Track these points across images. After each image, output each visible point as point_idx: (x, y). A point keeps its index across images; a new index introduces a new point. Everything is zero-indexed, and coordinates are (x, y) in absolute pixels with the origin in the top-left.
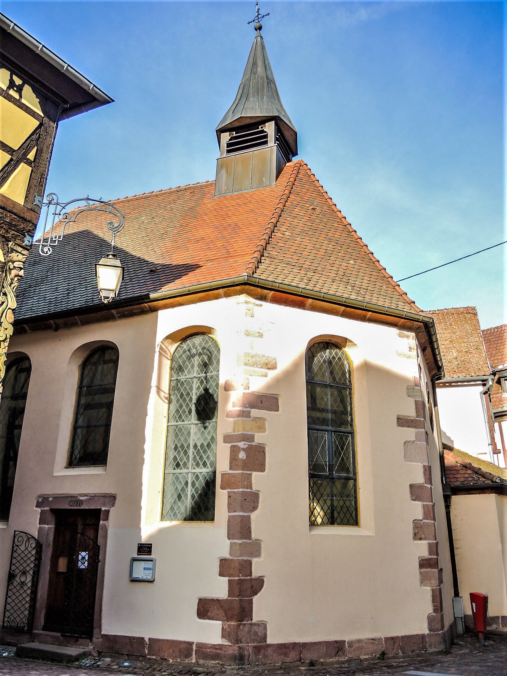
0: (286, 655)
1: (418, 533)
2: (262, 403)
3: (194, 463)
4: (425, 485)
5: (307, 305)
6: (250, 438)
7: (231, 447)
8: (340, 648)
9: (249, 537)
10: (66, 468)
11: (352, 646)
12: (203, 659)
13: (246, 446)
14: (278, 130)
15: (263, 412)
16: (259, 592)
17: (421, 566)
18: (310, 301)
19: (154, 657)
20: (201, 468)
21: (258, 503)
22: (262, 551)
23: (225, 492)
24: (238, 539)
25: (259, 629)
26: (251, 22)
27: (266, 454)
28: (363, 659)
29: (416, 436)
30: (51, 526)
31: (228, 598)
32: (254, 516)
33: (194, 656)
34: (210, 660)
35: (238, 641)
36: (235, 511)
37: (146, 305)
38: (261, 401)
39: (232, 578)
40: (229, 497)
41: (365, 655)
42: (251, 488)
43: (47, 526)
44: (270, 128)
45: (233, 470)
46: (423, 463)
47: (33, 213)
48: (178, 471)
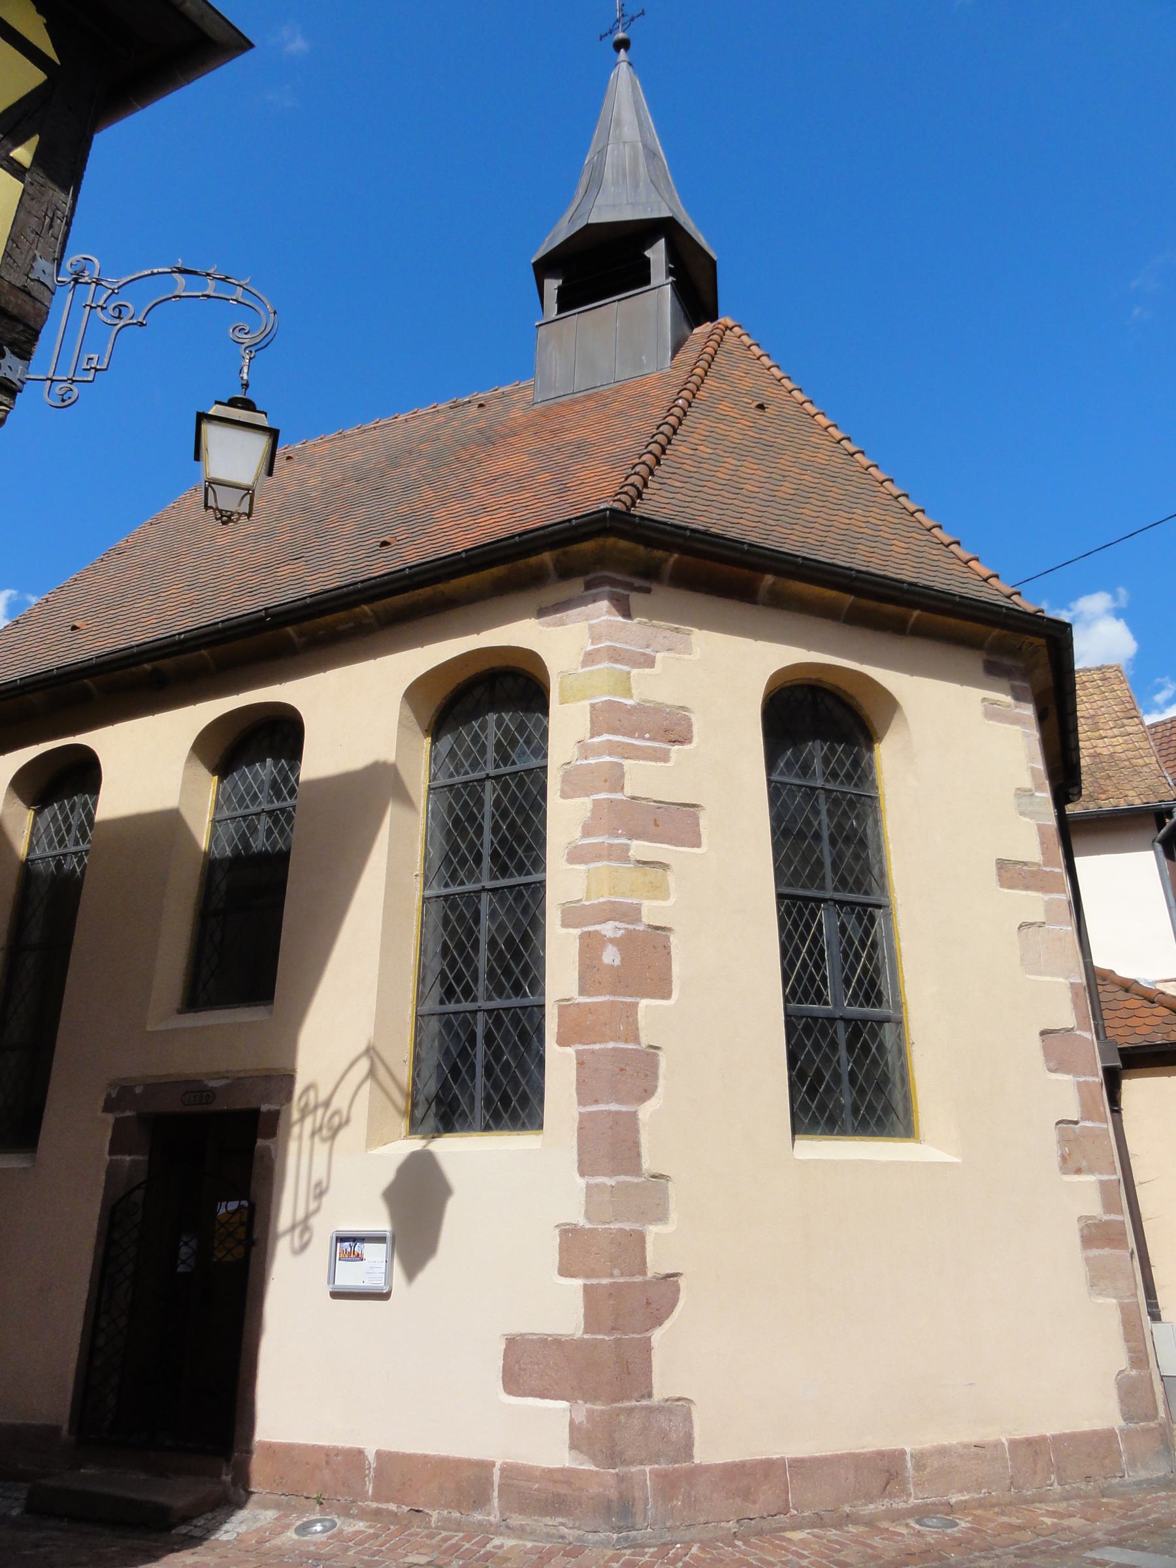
0: (747, 1495)
1: (1069, 1155)
2: (657, 825)
3: (489, 986)
4: (1078, 1032)
5: (762, 594)
6: (630, 914)
7: (582, 937)
8: (892, 1471)
9: (636, 1169)
10: (181, 1013)
11: (924, 1467)
12: (522, 1511)
13: (619, 933)
14: (673, 254)
15: (661, 848)
16: (667, 1318)
17: (1088, 1241)
18: (769, 579)
19: (392, 1507)
20: (509, 997)
21: (657, 1078)
22: (672, 1205)
23: (570, 1051)
24: (603, 1175)
25: (671, 1421)
26: (606, 35)
27: (673, 953)
28: (956, 1502)
29: (1047, 911)
30: (140, 1158)
31: (586, 1336)
32: (646, 1111)
33: (496, 1502)
34: (540, 1515)
35: (613, 1456)
36: (596, 1102)
37: (366, 608)
38: (655, 820)
39: (595, 1281)
40: (581, 1064)
41: (961, 1491)
42: (636, 1040)
43: (128, 1158)
44: (657, 254)
45: (590, 995)
46: (1069, 977)
47: (27, 298)
48: (451, 1007)
